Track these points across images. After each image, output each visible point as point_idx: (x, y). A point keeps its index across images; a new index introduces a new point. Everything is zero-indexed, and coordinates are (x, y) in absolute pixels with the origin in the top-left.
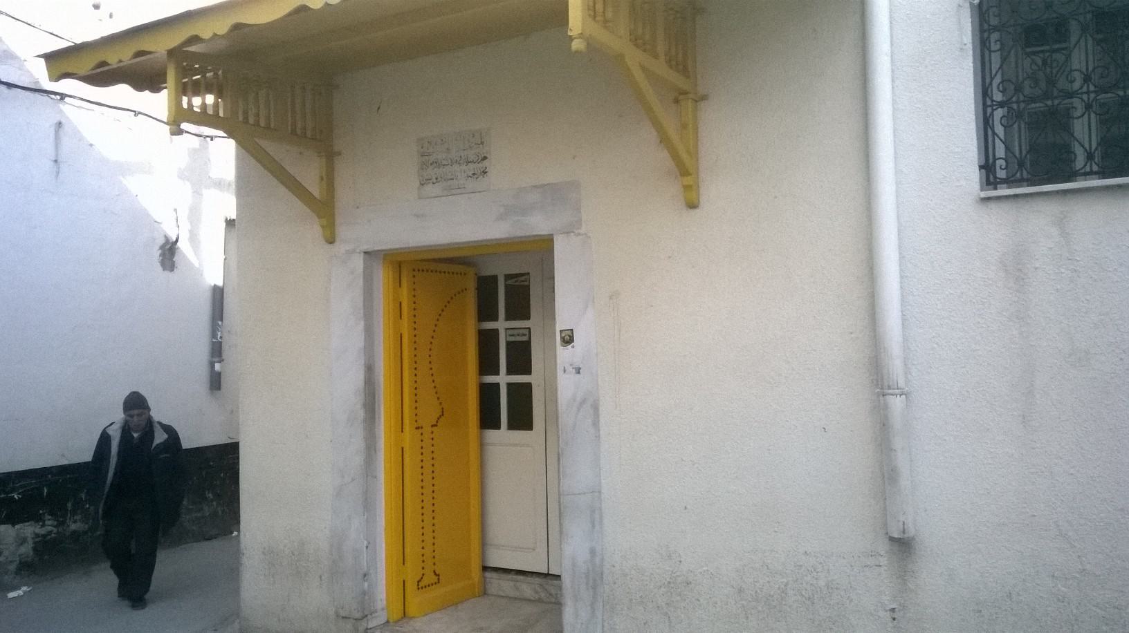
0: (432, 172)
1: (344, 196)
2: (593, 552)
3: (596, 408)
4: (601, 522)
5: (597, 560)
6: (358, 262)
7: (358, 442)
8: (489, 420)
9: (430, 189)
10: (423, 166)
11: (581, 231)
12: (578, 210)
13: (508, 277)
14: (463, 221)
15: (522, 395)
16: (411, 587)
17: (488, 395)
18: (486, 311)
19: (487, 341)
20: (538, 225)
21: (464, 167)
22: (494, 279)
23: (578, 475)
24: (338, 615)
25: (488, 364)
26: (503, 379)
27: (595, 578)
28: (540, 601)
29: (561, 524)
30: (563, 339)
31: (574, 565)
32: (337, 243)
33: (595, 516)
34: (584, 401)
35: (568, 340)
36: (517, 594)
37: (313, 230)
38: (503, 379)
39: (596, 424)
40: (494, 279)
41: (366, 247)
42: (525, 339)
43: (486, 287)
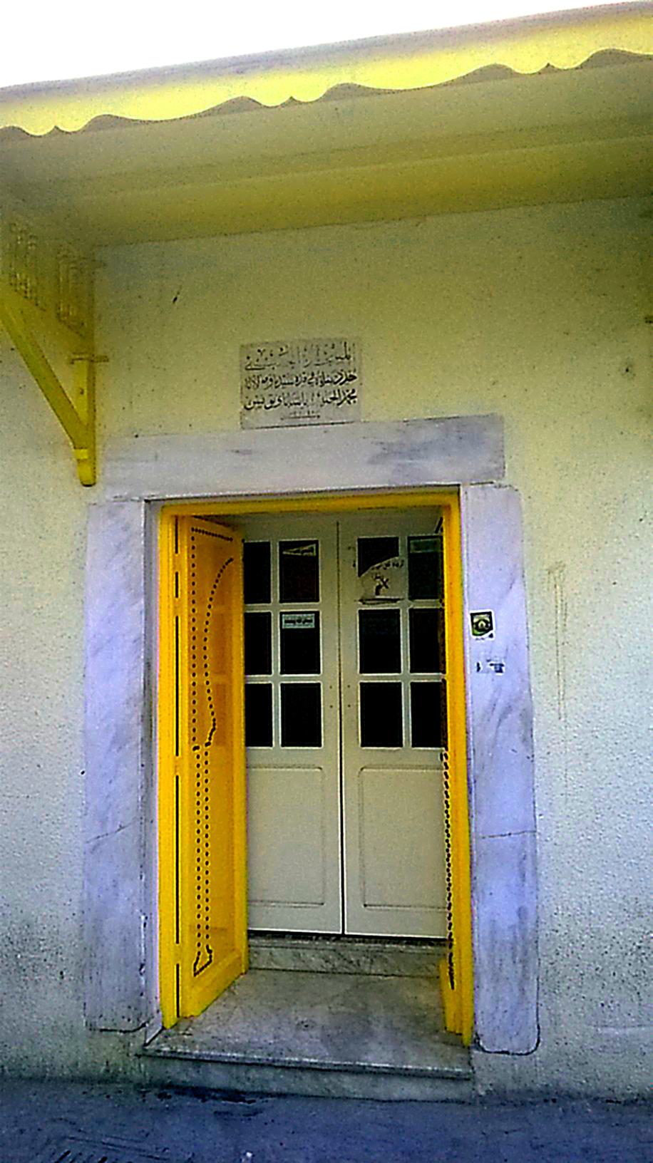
0: (265, 392)
1: (112, 417)
2: (521, 912)
3: (527, 719)
4: (535, 874)
5: (530, 925)
6: (137, 515)
7: (132, 772)
8: (257, 734)
9: (262, 416)
10: (249, 384)
11: (503, 482)
12: (500, 453)
13: (284, 546)
14: (309, 464)
15: (431, 706)
16: (187, 974)
17: (257, 699)
18: (256, 590)
19: (257, 629)
20: (438, 471)
21: (316, 388)
22: (265, 547)
23: (501, 807)
24: (91, 1027)
25: (257, 660)
26: (405, 677)
27: (525, 945)
28: (334, 972)
29: (472, 878)
30: (475, 626)
31: (493, 932)
32: (99, 487)
33: (526, 866)
34: (509, 709)
35: (483, 626)
36: (300, 966)
37: (60, 468)
38: (276, 679)
39: (527, 740)
40: (265, 547)
41: (147, 494)
42: (312, 625)
43: (256, 557)
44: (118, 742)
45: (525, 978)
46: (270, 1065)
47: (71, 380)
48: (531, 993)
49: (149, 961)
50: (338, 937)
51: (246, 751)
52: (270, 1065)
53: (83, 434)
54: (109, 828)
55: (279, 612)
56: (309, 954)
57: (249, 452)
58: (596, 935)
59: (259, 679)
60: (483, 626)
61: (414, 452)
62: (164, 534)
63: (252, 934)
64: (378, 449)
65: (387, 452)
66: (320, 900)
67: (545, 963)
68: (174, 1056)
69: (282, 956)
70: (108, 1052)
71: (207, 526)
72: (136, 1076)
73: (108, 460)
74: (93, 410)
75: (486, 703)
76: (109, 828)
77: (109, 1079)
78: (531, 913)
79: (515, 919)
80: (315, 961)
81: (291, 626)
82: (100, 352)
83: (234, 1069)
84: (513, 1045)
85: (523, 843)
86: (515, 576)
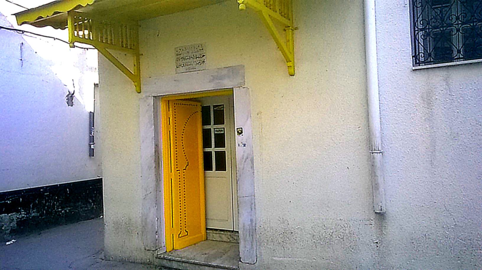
1: (144, 73)
6: (151, 101)
8: (208, 166)
9: (182, 69)
13: (214, 106)
14: (196, 83)
15: (221, 157)
17: (207, 156)
18: (206, 121)
19: (206, 134)
20: (227, 84)
23: (245, 189)
25: (207, 143)
26: (213, 150)
30: (238, 132)
33: (252, 206)
36: (221, 240)
37: (132, 87)
38: (213, 150)
39: (252, 167)
41: (153, 95)
43: (205, 111)
44: (149, 168)
45: (253, 240)
46: (187, 262)
47: (130, 64)
48: (254, 246)
49: (159, 231)
50: (233, 231)
51: (204, 173)
52: (187, 262)
53: (136, 78)
54: (148, 193)
55: (213, 127)
56: (223, 236)
57: (178, 81)
58: (272, 228)
59: (208, 150)
60: (240, 133)
61: (221, 78)
62: (162, 107)
63: (207, 229)
64: (212, 78)
65: (214, 78)
66: (227, 219)
67: (258, 236)
68: (164, 258)
69: (216, 236)
70: (148, 257)
71: (180, 102)
72: (156, 264)
73: (144, 85)
74: (139, 69)
75: (241, 156)
76: (148, 193)
77: (149, 264)
78: (254, 220)
79: (250, 223)
80: (225, 238)
81: (216, 132)
82: (141, 53)
83: (179, 263)
84: (250, 261)
85: (252, 200)
86: (249, 116)
